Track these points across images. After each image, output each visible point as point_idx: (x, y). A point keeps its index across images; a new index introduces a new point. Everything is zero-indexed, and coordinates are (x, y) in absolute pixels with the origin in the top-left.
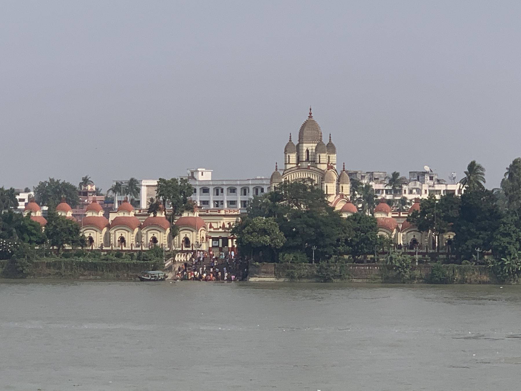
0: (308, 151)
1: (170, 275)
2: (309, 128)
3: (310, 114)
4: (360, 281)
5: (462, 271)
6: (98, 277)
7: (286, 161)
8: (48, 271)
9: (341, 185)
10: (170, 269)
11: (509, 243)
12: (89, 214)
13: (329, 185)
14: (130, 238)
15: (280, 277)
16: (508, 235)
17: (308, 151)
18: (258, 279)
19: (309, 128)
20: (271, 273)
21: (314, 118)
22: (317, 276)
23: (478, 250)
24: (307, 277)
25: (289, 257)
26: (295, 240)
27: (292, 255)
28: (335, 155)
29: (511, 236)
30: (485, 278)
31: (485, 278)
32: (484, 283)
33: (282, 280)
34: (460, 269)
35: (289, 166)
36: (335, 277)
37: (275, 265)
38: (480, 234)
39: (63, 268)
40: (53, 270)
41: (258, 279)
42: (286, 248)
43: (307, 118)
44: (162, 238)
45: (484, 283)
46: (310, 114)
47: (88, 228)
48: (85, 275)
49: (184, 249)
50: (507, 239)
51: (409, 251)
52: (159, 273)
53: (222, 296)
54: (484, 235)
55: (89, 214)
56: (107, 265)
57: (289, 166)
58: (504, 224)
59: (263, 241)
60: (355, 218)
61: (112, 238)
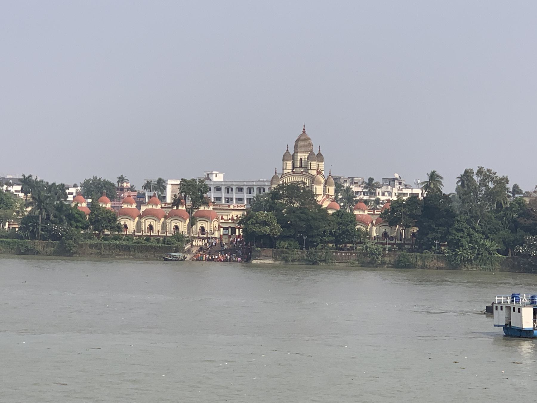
0: (301, 159)
1: (189, 257)
2: (303, 141)
3: (304, 130)
4: (341, 264)
5: (423, 259)
6: (131, 257)
7: (283, 167)
8: (91, 251)
9: (327, 188)
10: (189, 251)
11: (462, 237)
12: (125, 206)
13: (317, 187)
14: (157, 226)
15: (277, 260)
16: (461, 230)
17: (301, 159)
18: (259, 261)
19: (303, 141)
20: (270, 256)
21: (307, 133)
22: (306, 260)
23: (437, 242)
24: (299, 261)
25: (285, 244)
26: (289, 231)
27: (287, 243)
28: (323, 163)
29: (463, 231)
30: (442, 265)
31: (442, 265)
32: (441, 268)
33: (278, 262)
34: (422, 257)
35: (286, 171)
36: (321, 261)
37: (273, 250)
38: (438, 229)
39: (103, 249)
40: (94, 250)
41: (259, 261)
42: (282, 237)
43: (301, 133)
44: (183, 227)
45: (441, 268)
46: (304, 130)
47: (174, 218)
48: (120, 255)
49: (200, 236)
50: (460, 234)
51: (381, 242)
52: (180, 255)
53: (227, 276)
54: (441, 229)
55: (125, 206)
56: (139, 248)
57: (286, 171)
58: (458, 221)
59: (264, 231)
60: (338, 214)
61: (143, 226)
